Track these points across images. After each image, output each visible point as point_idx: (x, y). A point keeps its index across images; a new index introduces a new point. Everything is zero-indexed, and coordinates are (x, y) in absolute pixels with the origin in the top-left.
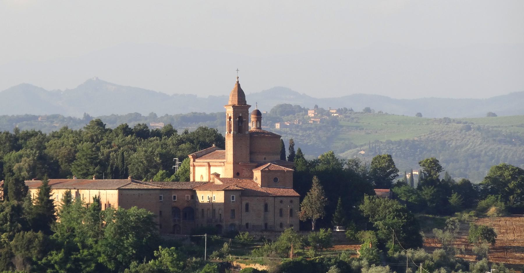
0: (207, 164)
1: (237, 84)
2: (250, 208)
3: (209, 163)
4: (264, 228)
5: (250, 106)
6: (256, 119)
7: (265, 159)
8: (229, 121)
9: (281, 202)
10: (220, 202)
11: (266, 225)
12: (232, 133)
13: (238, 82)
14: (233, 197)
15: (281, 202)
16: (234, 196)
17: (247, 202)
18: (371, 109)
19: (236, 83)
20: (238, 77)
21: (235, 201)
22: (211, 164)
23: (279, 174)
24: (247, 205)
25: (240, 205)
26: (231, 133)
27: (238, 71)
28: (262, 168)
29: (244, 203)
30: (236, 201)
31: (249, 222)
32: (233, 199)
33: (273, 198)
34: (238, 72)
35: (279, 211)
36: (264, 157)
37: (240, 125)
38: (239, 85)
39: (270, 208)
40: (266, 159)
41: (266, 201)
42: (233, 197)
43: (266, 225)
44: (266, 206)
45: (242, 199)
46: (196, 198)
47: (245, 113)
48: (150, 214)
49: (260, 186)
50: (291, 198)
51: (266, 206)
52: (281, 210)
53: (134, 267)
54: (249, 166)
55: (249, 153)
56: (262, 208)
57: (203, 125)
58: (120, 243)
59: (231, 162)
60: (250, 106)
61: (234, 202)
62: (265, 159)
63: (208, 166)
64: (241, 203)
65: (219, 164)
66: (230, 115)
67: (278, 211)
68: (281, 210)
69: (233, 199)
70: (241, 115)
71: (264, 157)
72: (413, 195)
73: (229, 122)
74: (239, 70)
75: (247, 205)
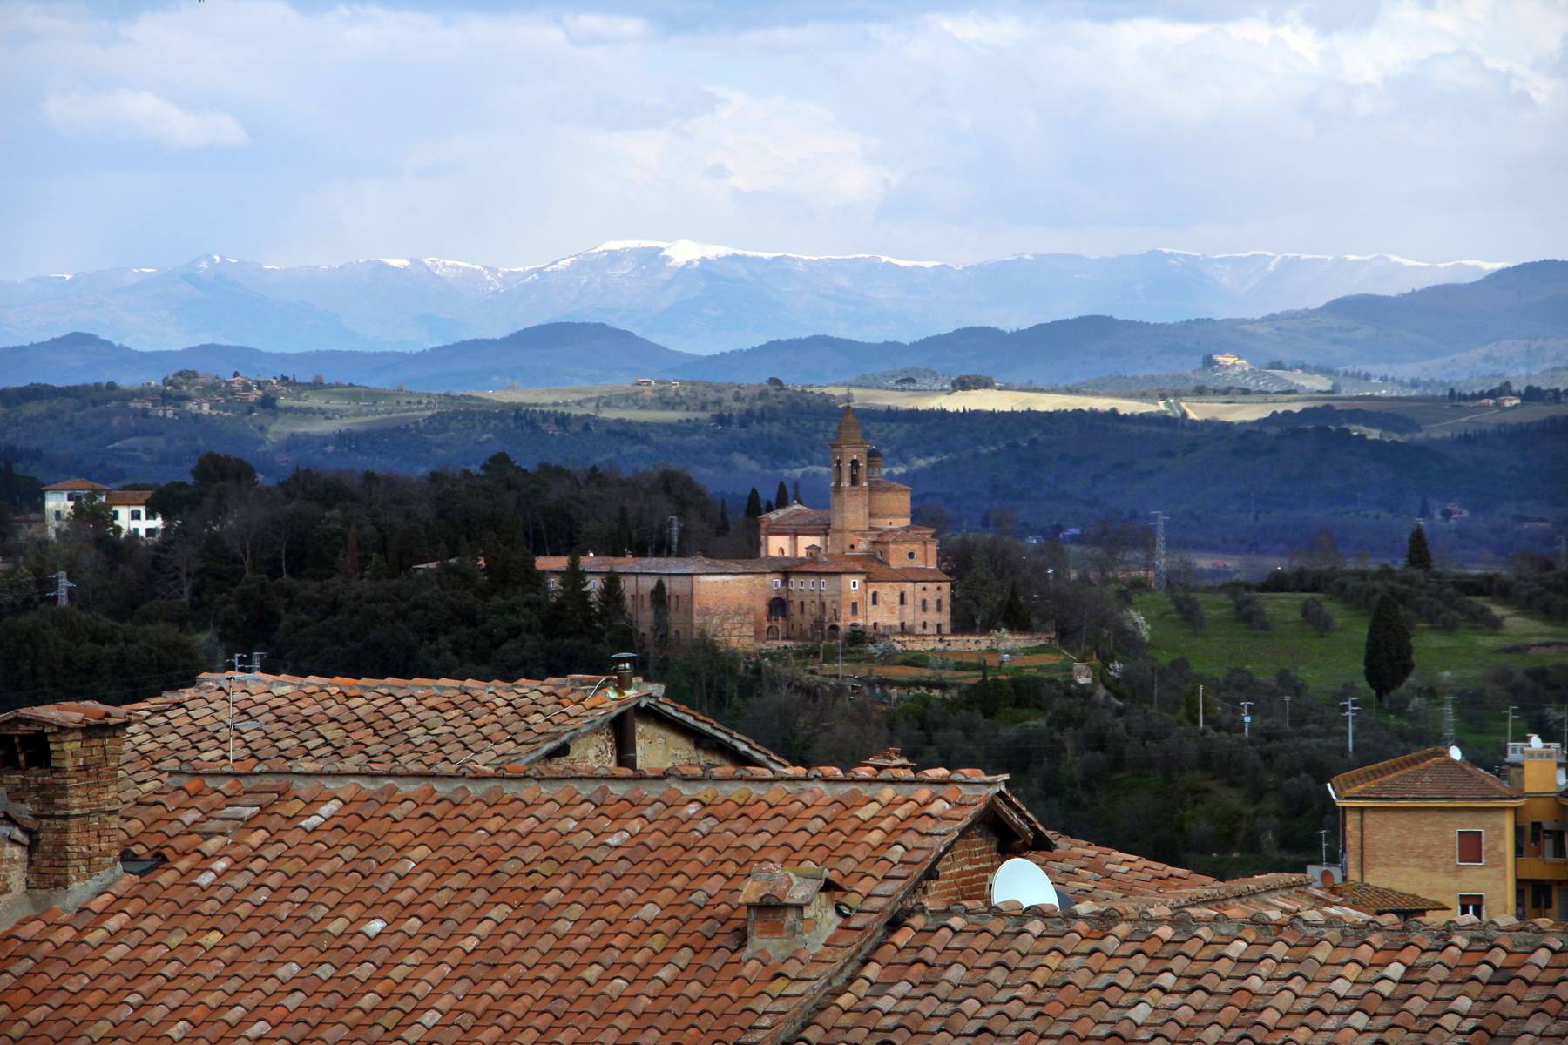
2: (879, 598)
4: (899, 629)
7: (891, 523)
11: (903, 624)
14: (854, 583)
15: (924, 589)
18: (774, 595)
24: (875, 595)
29: (870, 592)
31: (878, 621)
32: (854, 585)
35: (920, 604)
37: (855, 472)
39: (909, 599)
42: (854, 583)
43: (903, 624)
44: (902, 595)
46: (1155, 429)
48: (1384, 442)
51: (902, 595)
52: (924, 602)
55: (867, 515)
56: (897, 599)
57: (764, 544)
62: (891, 523)
67: (919, 603)
68: (924, 602)
69: (854, 585)
70: (855, 457)
71: (889, 521)
72: (79, 736)
75: (875, 595)
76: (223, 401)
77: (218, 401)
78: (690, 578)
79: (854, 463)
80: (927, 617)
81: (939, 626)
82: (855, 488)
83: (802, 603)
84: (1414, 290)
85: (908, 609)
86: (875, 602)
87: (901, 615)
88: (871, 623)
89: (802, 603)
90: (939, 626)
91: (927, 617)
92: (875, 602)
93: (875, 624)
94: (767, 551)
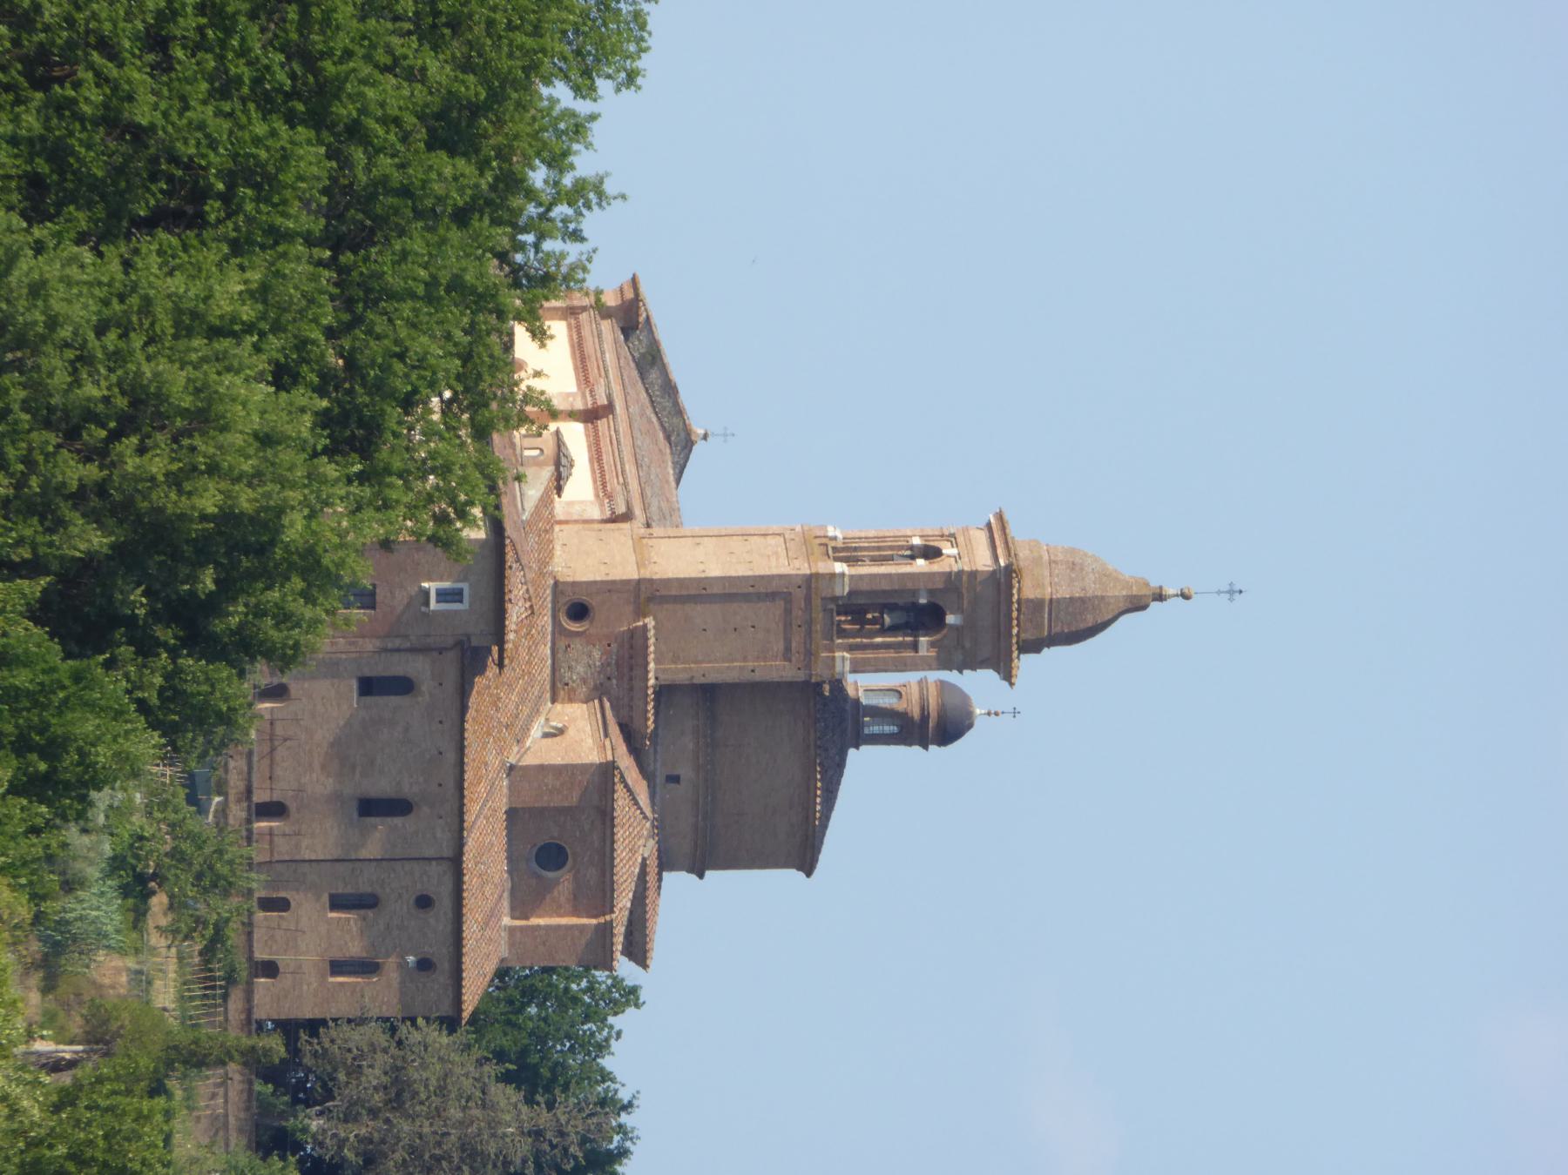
0: (603, 401)
1: (1144, 592)
3: (609, 409)
5: (1008, 676)
6: (916, 713)
7: (674, 779)
8: (911, 548)
9: (424, 902)
10: (687, 576)
12: (839, 567)
13: (1160, 597)
16: (461, 601)
17: (424, 688)
19: (1154, 583)
20: (1185, 596)
21: (433, 605)
22: (602, 424)
23: (592, 874)
24: (403, 686)
25: (408, 645)
26: (837, 559)
27: (1231, 592)
28: (626, 763)
30: (429, 617)
33: (447, 852)
34: (1219, 592)
36: (685, 771)
38: (1137, 605)
40: (672, 786)
41: (426, 810)
44: (397, 807)
45: (441, 651)
47: (968, 645)
49: (512, 760)
50: (445, 966)
51: (397, 807)
53: (70, 369)
54: (631, 679)
56: (381, 787)
58: (49, 812)
59: (656, 568)
60: (1008, 676)
61: (427, 603)
62: (674, 779)
63: (590, 406)
64: (413, 650)
65: (614, 484)
66: (948, 550)
70: (950, 619)
71: (685, 771)
73: (901, 548)
74: (1231, 600)
75: (403, 686)
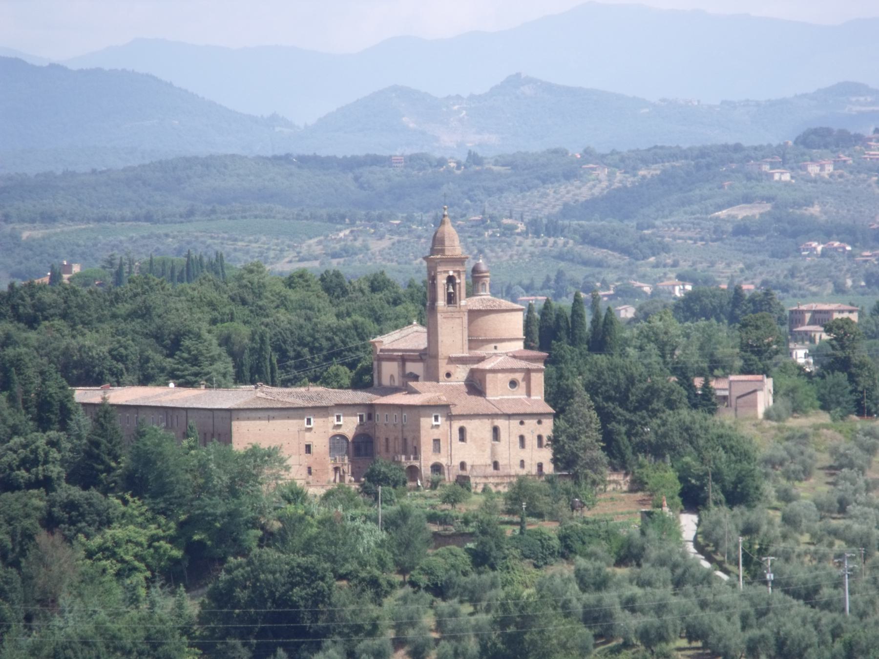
7: (496, 348)
24: (462, 431)
35: (518, 439)
37: (451, 290)
39: (503, 434)
52: (522, 438)
68: (522, 438)
76: (851, 162)
77: (845, 161)
78: (229, 413)
79: (451, 280)
80: (525, 454)
81: (540, 466)
82: (450, 309)
83: (387, 440)
84: (262, 116)
85: (502, 447)
86: (462, 438)
87: (493, 453)
88: (456, 463)
89: (387, 440)
90: (540, 466)
91: (525, 454)
92: (462, 438)
93: (463, 465)
94: (379, 378)
